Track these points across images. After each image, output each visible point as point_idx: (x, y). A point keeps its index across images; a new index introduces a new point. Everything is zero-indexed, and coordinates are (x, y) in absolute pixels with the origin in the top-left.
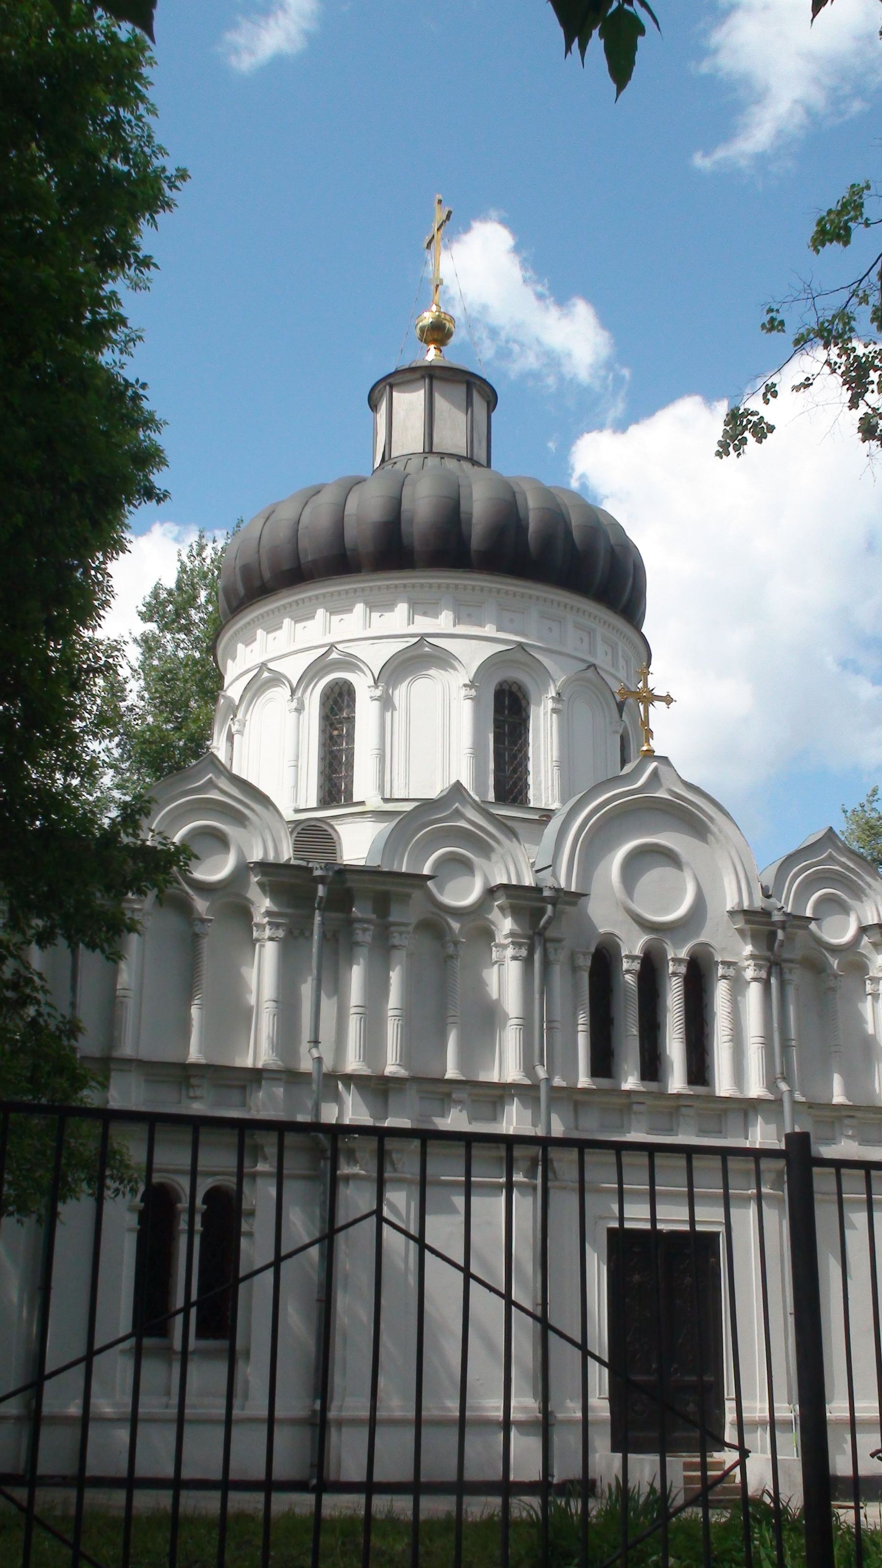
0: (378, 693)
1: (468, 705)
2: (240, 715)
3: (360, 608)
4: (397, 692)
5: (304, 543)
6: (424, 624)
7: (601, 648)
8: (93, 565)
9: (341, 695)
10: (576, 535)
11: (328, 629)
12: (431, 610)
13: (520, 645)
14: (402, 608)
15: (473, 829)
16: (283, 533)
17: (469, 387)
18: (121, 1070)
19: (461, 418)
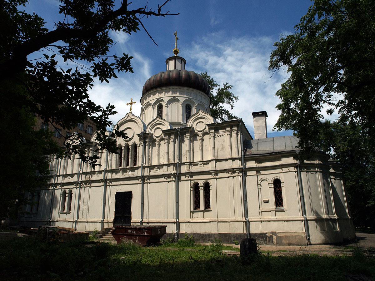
2: (144, 110)
3: (164, 93)
5: (163, 80)
6: (174, 95)
7: (203, 99)
8: (71, 148)
9: (160, 106)
10: (200, 82)
11: (158, 96)
12: (175, 92)
14: (171, 92)
15: (312, 162)
16: (159, 78)
18: (116, 159)
19: (180, 65)
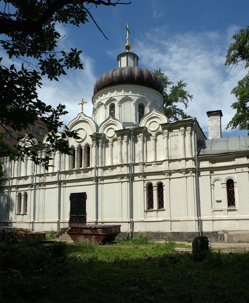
0: (119, 105)
1: (134, 107)
2: (96, 110)
4: (122, 105)
6: (126, 94)
11: (110, 95)
13: (143, 97)
14: (123, 91)
17: (134, 56)
